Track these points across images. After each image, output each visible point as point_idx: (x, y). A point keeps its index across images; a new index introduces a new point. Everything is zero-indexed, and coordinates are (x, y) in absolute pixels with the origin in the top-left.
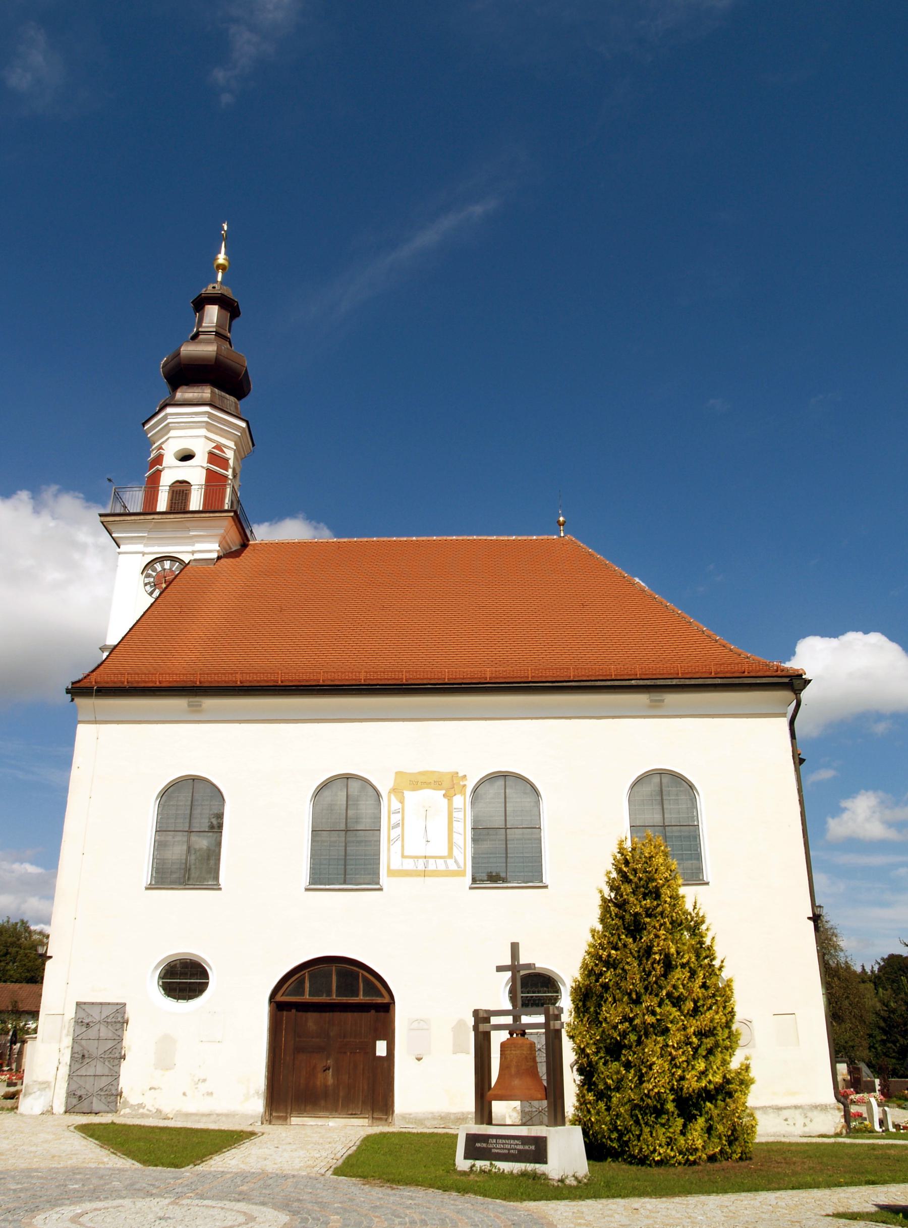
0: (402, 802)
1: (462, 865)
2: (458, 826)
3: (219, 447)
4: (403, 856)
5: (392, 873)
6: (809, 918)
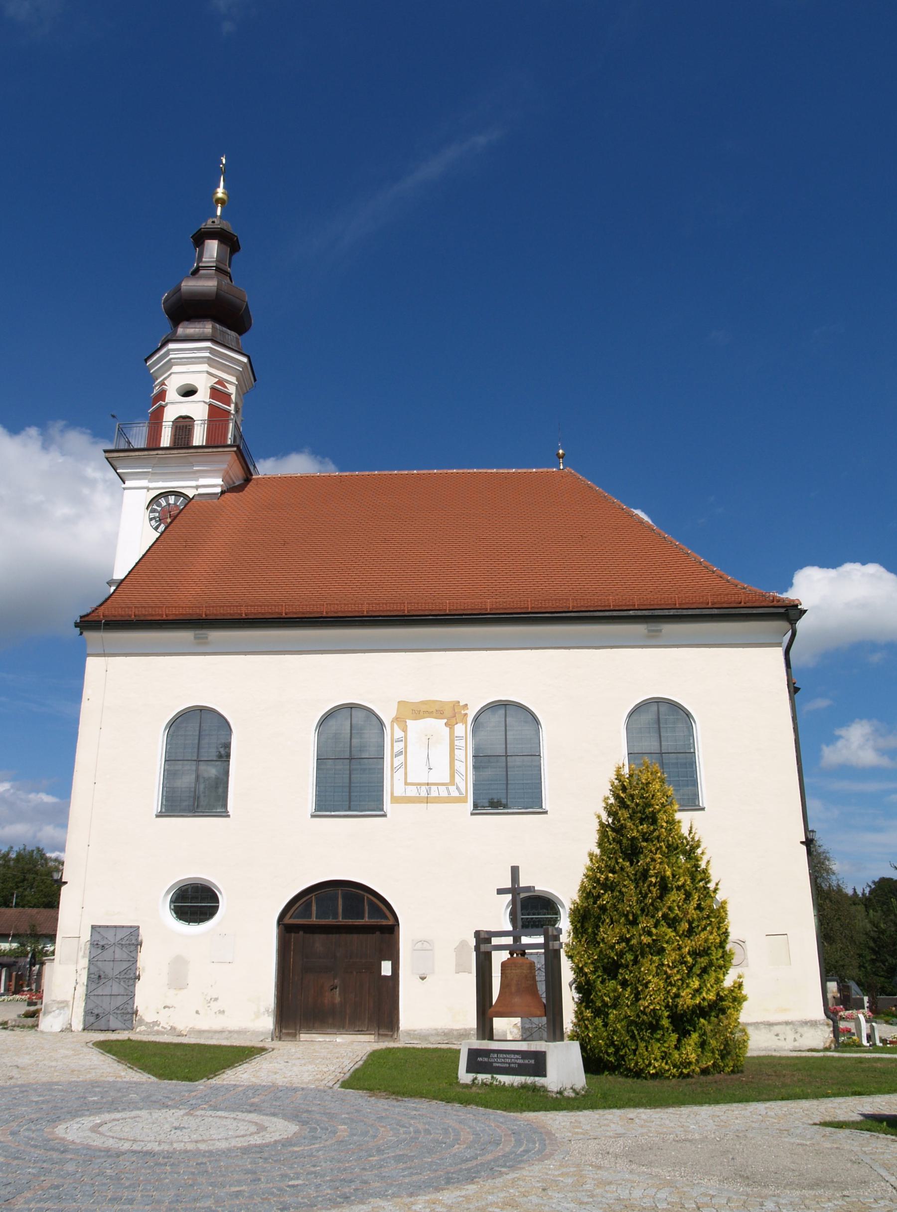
0: (405, 730)
1: (463, 791)
3: (221, 382)
4: (406, 783)
5: (395, 800)
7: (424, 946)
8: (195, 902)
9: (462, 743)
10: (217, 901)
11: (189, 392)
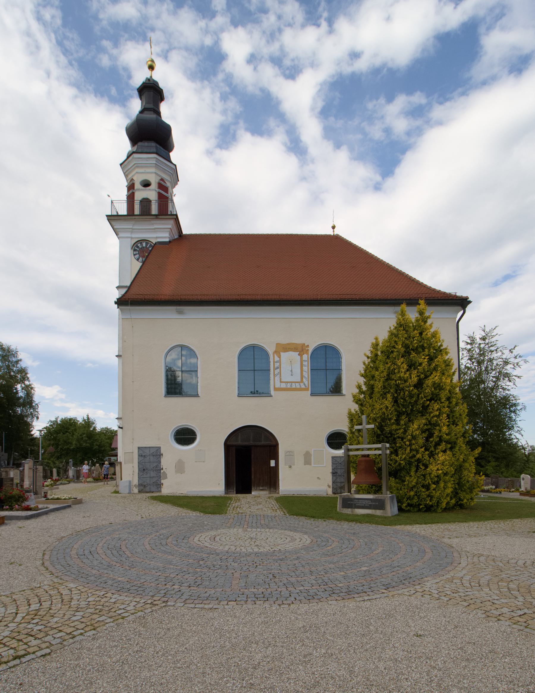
0: (280, 357)
1: (307, 385)
2: (305, 368)
3: (162, 180)
4: (281, 382)
5: (276, 389)
6: (455, 8)
7: (290, 454)
8: (185, 436)
9: (306, 363)
10: (196, 435)
11: (146, 184)
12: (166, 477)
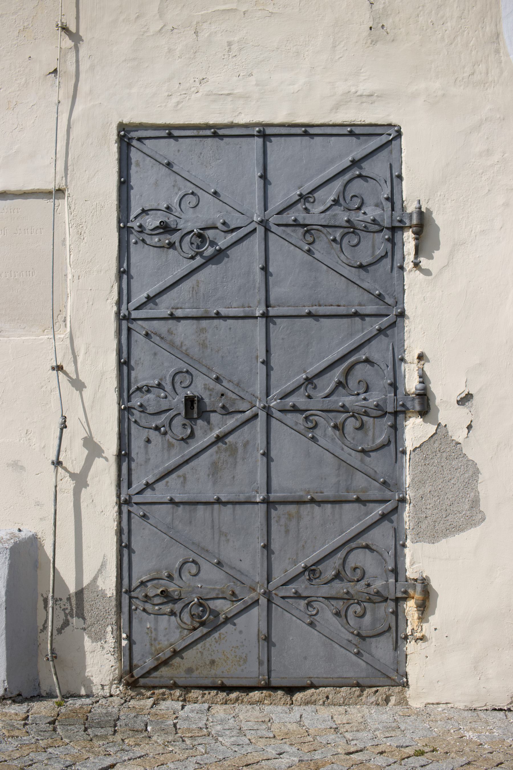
12: (463, 512)
